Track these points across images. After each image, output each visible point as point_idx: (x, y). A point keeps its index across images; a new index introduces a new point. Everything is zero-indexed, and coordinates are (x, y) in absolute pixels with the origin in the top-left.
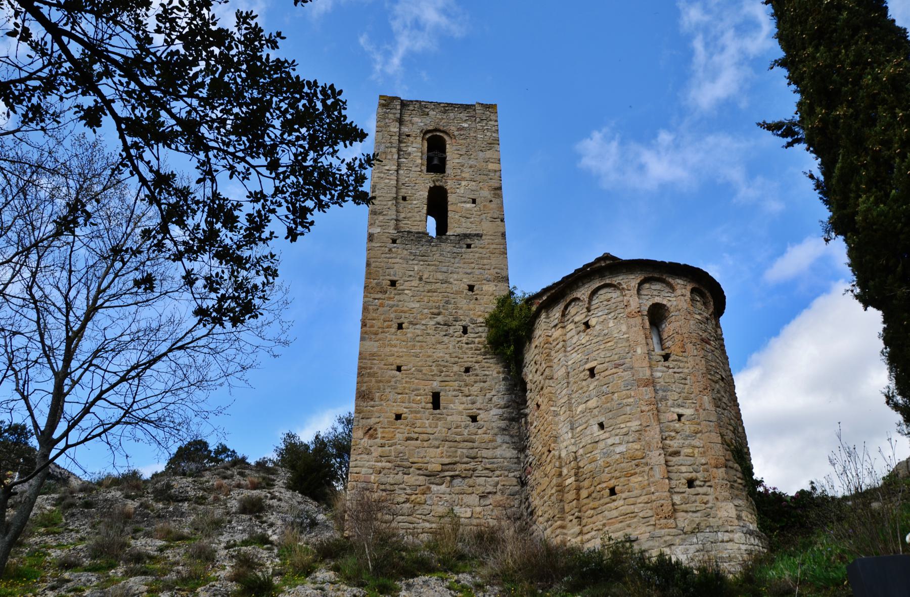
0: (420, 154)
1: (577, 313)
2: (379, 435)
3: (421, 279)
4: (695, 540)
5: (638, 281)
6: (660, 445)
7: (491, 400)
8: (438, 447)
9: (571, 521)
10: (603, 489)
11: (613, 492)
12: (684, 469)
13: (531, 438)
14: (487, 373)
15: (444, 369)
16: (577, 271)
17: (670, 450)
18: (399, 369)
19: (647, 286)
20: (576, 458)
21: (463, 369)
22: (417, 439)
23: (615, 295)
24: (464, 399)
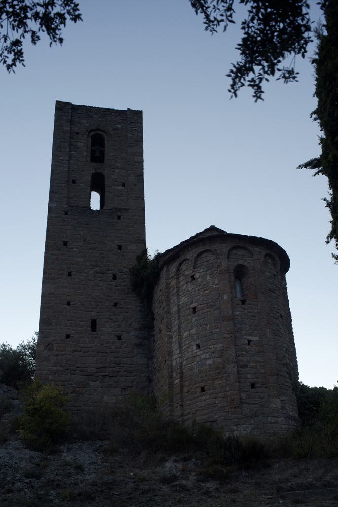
0: (85, 148)
1: (187, 270)
2: (55, 349)
3: (84, 241)
4: (253, 422)
5: (228, 249)
6: (235, 360)
7: (131, 325)
8: (94, 357)
9: (177, 407)
10: (196, 388)
11: (203, 390)
12: (249, 376)
13: (156, 352)
14: (129, 306)
15: (100, 304)
16: (191, 238)
17: (241, 363)
18: (69, 304)
19: (234, 252)
20: (181, 366)
21: (112, 304)
22: (80, 351)
23: (211, 258)
24: (113, 324)
